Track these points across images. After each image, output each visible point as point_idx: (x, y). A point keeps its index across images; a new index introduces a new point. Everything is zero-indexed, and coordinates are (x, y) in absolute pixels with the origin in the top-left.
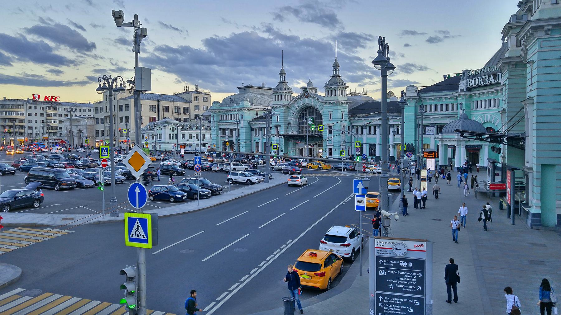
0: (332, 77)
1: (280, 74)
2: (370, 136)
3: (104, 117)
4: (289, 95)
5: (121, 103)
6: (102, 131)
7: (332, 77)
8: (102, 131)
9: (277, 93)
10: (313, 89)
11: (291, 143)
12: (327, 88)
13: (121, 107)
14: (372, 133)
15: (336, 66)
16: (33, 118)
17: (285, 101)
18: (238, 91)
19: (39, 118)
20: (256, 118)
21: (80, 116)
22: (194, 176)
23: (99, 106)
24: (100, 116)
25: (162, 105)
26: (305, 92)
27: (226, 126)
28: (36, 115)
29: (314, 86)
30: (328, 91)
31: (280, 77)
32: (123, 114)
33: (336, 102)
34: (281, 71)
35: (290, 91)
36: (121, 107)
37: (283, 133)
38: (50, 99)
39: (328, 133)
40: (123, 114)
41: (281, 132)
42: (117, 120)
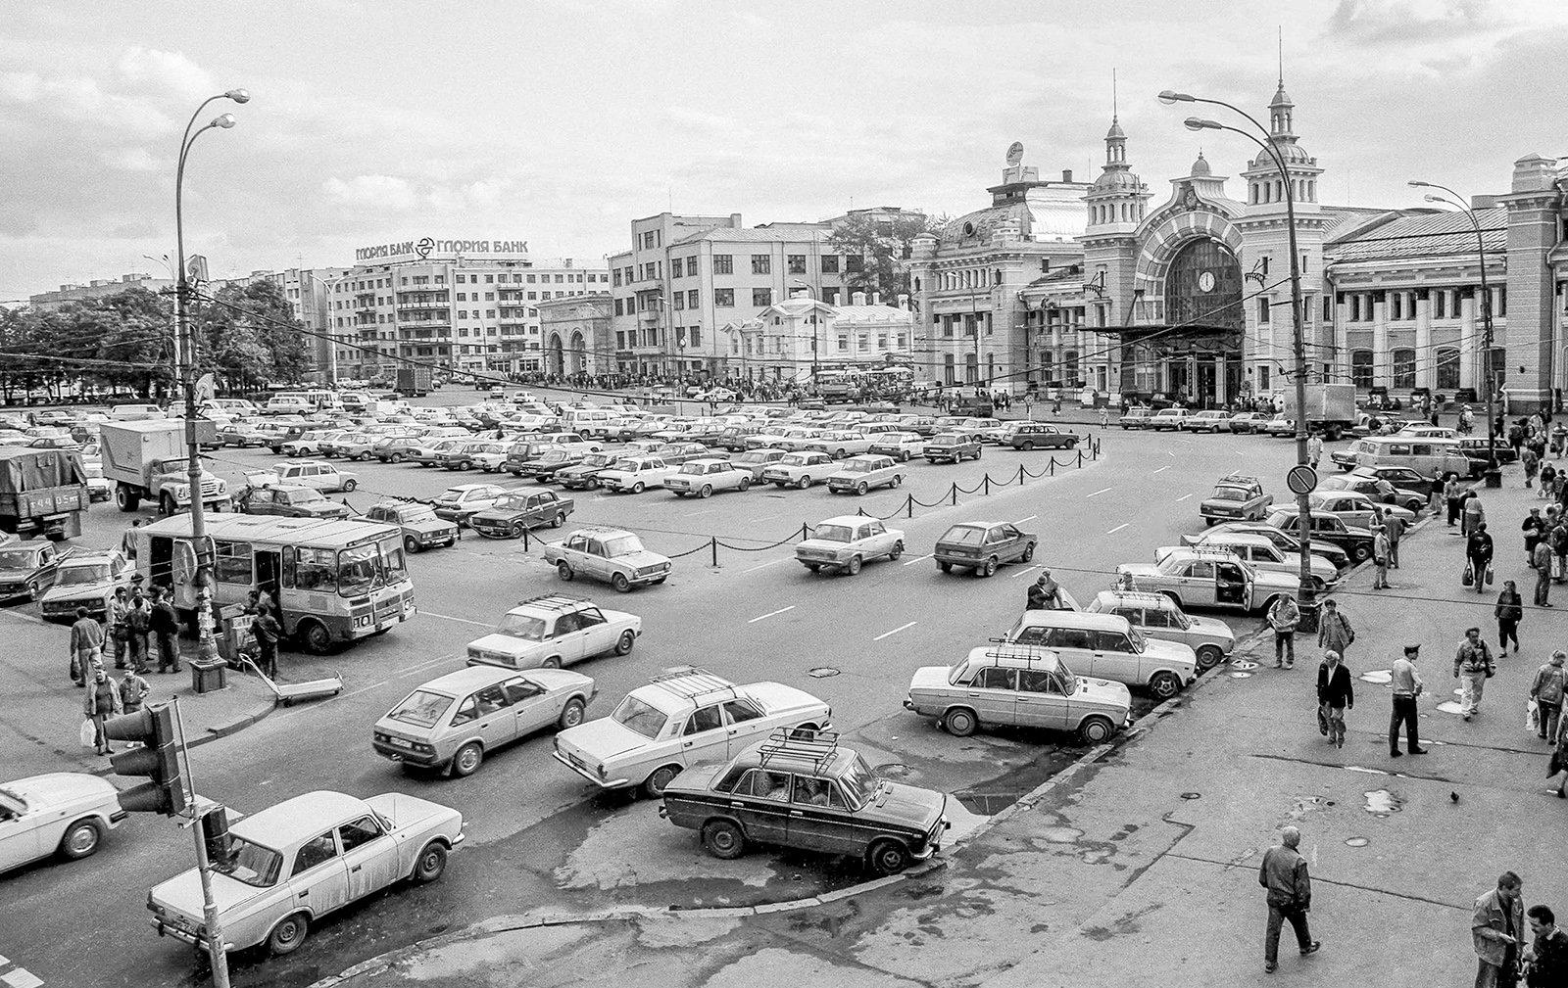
0: (1105, 169)
1: (1108, 140)
2: (1355, 325)
3: (635, 295)
4: (1306, 180)
5: (675, 254)
6: (632, 334)
7: (1105, 169)
8: (632, 334)
9: (1100, 200)
10: (1210, 181)
11: (1143, 348)
12: (1252, 177)
13: (677, 264)
14: (1362, 315)
15: (1282, 106)
16: (469, 306)
17: (1126, 226)
18: (988, 201)
19: (483, 305)
20: (1042, 280)
21: (581, 293)
22: (1314, 603)
23: (622, 264)
24: (625, 292)
25: (458, 309)
26: (1186, 195)
27: (955, 304)
28: (475, 296)
29: (1216, 172)
30: (1268, 185)
31: (1109, 151)
32: (684, 284)
33: (1281, 222)
34: (1112, 131)
35: (1137, 194)
36: (677, 264)
37: (1117, 324)
38: (137, 636)
39: (1256, 319)
40: (684, 284)
41: (1115, 319)
42: (668, 300)
